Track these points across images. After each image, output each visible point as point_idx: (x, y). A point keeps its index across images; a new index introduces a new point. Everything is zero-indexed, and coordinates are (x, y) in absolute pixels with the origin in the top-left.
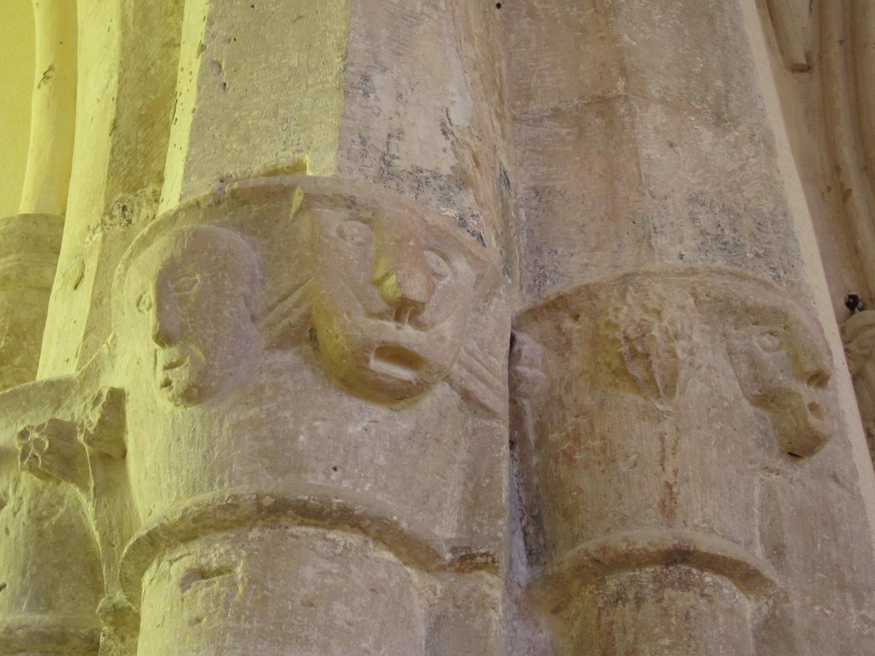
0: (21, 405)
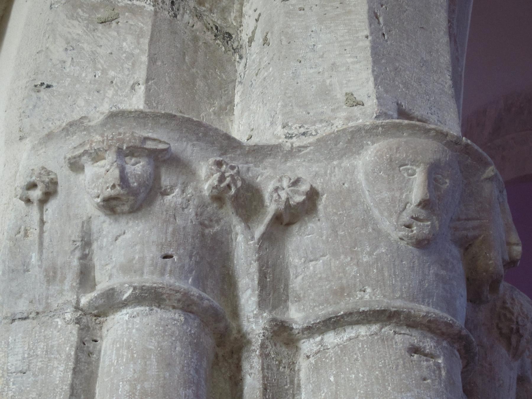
0: (198, 134)
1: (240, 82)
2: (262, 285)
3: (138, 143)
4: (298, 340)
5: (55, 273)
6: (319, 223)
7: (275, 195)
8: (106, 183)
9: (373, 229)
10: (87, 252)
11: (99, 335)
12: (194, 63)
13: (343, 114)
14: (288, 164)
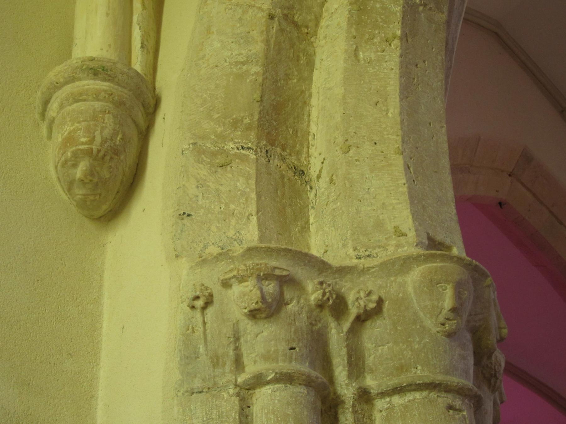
1: (313, 207)
2: (350, 364)
3: (270, 272)
4: (374, 399)
5: (218, 360)
6: (384, 321)
7: (356, 303)
8: (251, 300)
9: (420, 326)
10: (237, 345)
11: (251, 402)
12: (283, 194)
13: (394, 242)
14: (361, 279)
